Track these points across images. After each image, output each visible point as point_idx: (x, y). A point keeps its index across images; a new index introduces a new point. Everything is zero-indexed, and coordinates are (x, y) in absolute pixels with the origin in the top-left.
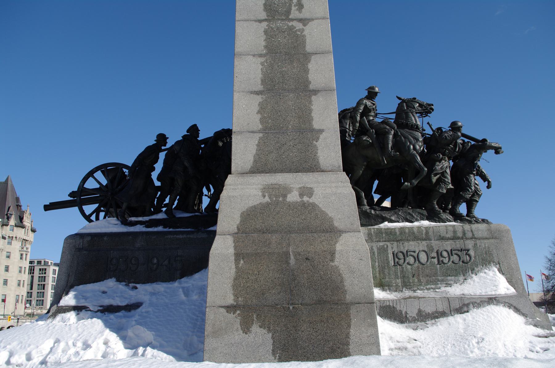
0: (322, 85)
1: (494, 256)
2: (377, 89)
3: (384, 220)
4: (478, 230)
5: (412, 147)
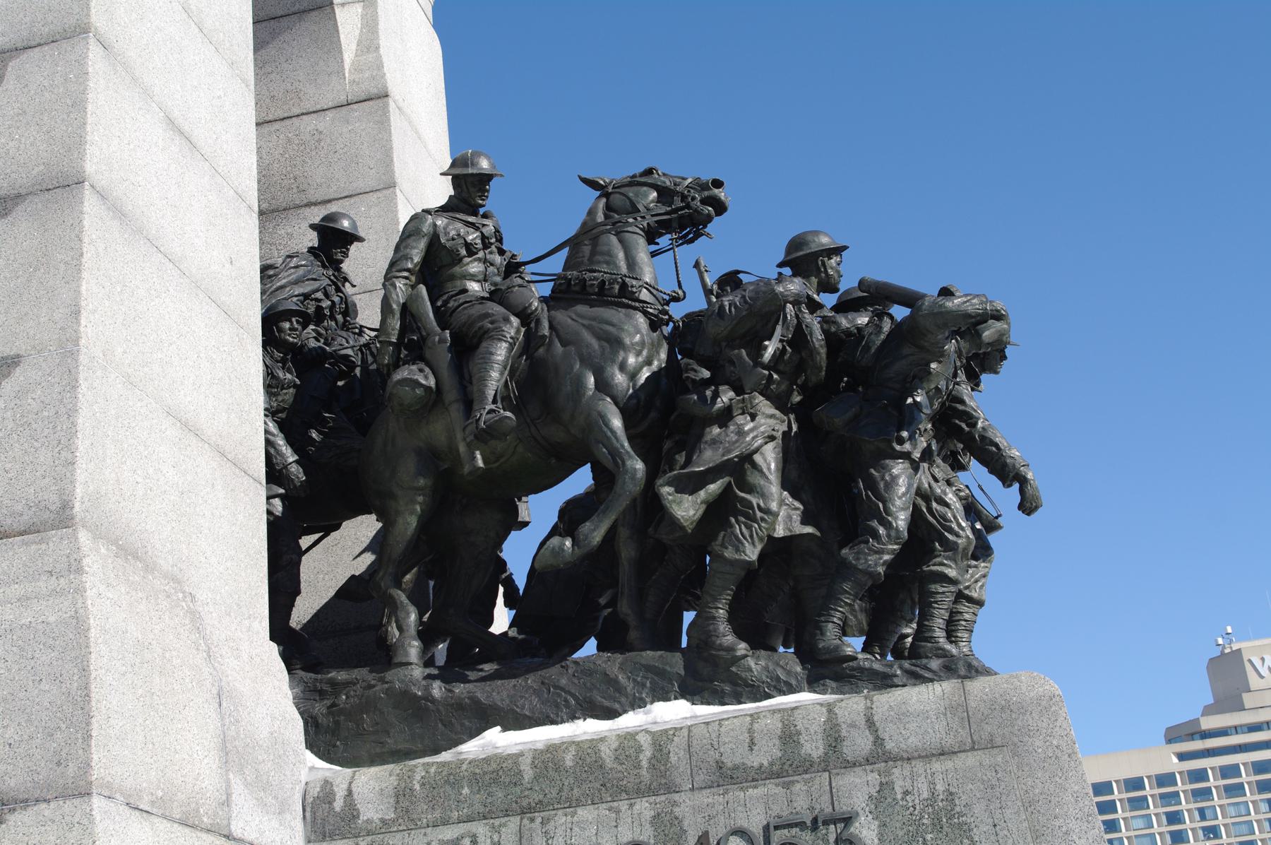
0: (37, 170)
1: (976, 838)
2: (484, 164)
3: (483, 718)
4: (902, 716)
5: (591, 380)
